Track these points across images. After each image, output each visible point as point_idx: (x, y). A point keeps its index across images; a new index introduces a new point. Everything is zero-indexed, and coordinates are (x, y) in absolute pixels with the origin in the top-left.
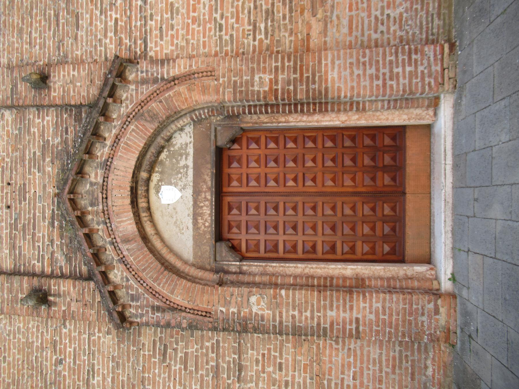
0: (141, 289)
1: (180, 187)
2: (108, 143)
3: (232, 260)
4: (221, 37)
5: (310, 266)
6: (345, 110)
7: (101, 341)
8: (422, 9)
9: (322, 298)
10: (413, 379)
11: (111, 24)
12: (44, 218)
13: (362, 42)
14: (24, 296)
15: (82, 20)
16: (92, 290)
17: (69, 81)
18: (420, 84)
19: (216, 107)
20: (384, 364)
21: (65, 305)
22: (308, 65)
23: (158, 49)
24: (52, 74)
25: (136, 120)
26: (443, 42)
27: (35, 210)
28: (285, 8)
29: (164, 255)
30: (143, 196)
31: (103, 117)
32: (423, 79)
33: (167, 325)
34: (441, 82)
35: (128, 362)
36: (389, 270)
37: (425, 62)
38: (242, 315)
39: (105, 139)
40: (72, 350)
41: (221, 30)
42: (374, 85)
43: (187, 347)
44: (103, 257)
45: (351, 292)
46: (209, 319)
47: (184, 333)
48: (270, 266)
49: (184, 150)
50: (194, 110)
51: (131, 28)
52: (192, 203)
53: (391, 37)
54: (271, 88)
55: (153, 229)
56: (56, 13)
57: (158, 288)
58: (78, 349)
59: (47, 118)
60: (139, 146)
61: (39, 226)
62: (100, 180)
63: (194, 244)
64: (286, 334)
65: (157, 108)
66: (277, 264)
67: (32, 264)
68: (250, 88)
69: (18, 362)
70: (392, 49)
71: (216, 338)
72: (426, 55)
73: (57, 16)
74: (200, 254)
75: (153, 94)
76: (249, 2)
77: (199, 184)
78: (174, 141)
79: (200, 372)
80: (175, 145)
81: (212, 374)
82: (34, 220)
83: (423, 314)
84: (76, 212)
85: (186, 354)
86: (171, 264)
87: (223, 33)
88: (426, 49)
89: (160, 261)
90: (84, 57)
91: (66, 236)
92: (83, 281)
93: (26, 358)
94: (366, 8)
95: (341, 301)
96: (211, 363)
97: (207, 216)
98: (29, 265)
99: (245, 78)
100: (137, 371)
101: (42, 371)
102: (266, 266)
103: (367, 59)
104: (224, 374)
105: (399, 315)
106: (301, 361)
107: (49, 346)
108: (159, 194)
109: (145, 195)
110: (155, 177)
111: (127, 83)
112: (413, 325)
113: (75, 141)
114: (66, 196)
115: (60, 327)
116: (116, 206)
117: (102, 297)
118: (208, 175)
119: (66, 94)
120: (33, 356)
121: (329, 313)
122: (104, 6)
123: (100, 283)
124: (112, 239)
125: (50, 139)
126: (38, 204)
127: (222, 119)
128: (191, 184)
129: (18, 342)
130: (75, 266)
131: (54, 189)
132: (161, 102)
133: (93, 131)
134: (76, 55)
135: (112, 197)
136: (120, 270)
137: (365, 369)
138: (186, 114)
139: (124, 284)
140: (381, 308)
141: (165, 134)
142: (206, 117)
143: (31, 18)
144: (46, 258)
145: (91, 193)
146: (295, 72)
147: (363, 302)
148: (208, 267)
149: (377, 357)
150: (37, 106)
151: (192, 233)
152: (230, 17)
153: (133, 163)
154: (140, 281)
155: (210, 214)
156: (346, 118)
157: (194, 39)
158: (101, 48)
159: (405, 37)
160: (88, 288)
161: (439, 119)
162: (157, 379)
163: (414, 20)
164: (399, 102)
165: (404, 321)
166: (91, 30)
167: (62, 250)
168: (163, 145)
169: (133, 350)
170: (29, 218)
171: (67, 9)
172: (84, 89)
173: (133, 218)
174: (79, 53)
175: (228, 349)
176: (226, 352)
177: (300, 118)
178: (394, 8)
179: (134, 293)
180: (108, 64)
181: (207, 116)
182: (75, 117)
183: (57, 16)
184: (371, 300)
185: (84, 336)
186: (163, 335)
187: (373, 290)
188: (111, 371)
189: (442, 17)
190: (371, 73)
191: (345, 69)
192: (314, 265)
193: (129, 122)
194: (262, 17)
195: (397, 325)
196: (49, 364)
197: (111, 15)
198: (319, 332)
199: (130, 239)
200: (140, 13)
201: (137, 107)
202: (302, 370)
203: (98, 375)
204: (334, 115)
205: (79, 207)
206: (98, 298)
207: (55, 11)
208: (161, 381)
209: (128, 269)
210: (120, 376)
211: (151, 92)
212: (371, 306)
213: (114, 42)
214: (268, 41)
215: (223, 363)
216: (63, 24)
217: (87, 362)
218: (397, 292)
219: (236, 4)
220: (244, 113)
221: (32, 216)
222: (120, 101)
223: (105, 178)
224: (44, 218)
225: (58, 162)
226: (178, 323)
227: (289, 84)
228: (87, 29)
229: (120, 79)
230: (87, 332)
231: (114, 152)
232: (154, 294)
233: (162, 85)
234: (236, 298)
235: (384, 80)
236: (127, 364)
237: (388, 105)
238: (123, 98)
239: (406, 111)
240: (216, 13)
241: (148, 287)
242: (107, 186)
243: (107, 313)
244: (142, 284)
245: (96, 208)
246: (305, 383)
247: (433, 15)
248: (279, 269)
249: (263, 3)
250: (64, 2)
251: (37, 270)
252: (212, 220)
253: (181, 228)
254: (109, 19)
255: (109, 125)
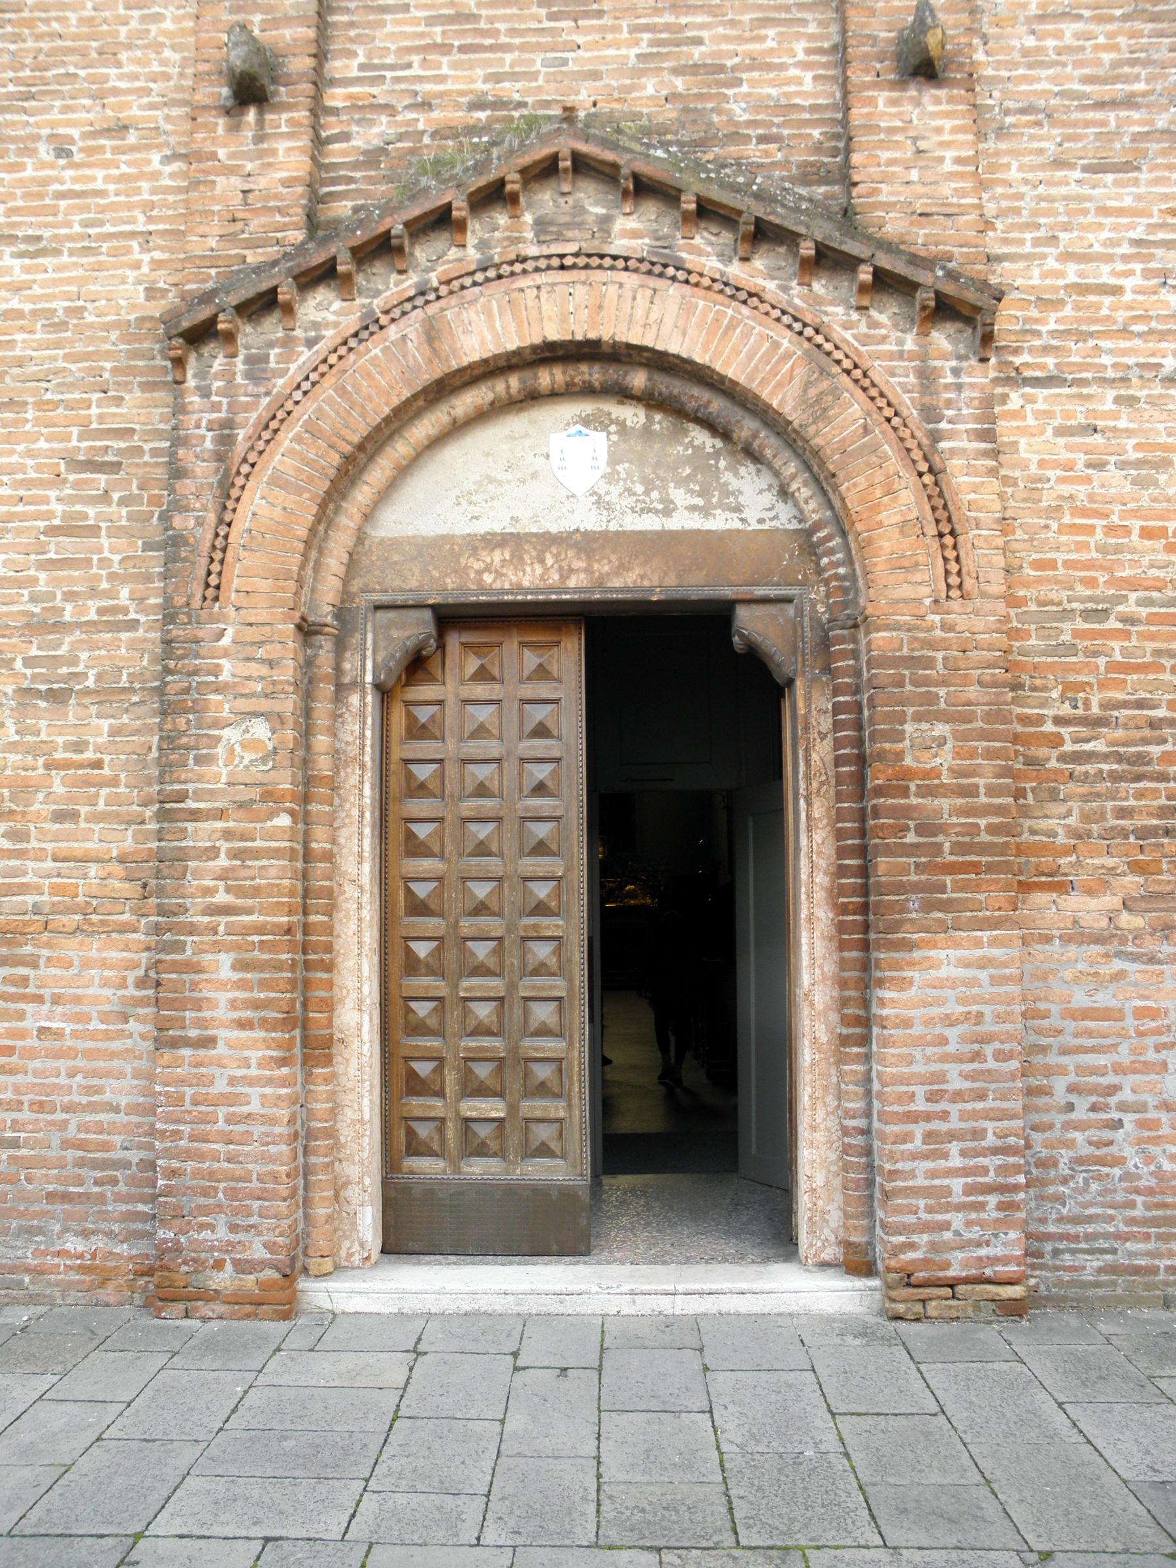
0: (284, 386)
1: (602, 492)
2: (735, 270)
3: (379, 659)
4: (1066, 615)
5: (366, 899)
6: (844, 1003)
7: (128, 272)
8: (1133, 1221)
9: (271, 937)
10: (51, 1197)
11: (1104, 275)
12: (497, 78)
13: (1044, 1050)
14: (256, 32)
15: (1116, 183)
16: (279, 235)
17: (922, 145)
18: (910, 1219)
19: (855, 602)
20: (89, 1118)
21: (232, 156)
22: (977, 888)
23: (1031, 421)
24: (942, 93)
25: (807, 353)
26: (1032, 1282)
27: (523, 48)
28: (1151, 814)
29: (389, 450)
30: (572, 378)
31: (813, 252)
32: (927, 1227)
33: (177, 470)
34: (913, 1280)
35: (66, 357)
36: (359, 1136)
37: (975, 1233)
38: (211, 697)
39: (745, 259)
40: (99, 185)
41: (1087, 615)
42: (912, 1088)
43: (116, 532)
44: (379, 267)
45: (287, 1023)
46: (199, 596)
47: (155, 520)
48: (362, 776)
49: (720, 500)
50: (843, 534)
51: (1091, 334)
52: (554, 529)
53: (1057, 1133)
54: (908, 774)
55: (471, 411)
56: (1139, 99)
57: (286, 439)
58: (102, 202)
59: (808, 76)
60: (727, 363)
61: (471, 66)
62: (618, 245)
63: (424, 538)
64: (160, 831)
65: (845, 419)
66: (368, 801)
67: (354, 47)
68: (910, 710)
69: (58, 19)
70: (1016, 1135)
71: (143, 619)
72: (996, 1236)
73: (1129, 102)
74: (396, 558)
75: (889, 404)
76: (1173, 705)
77: (614, 552)
78: (747, 469)
79: (43, 576)
80: (736, 474)
81: (37, 610)
82: (492, 48)
83: (234, 1228)
84: (517, 177)
85: (94, 531)
86: (362, 471)
87: (1081, 625)
88: (1013, 1235)
89: (368, 438)
90: (999, 190)
91: (442, 148)
92: (304, 207)
93: (69, 43)
94: (1142, 1059)
95: (262, 995)
96: (69, 607)
97: (514, 579)
98: (352, 40)
99: (942, 692)
100: (44, 385)
101: (30, 97)
102: (362, 766)
103: (991, 1064)
104: (39, 648)
105: (229, 1161)
106: (85, 876)
107: (109, 113)
108: (579, 427)
109: (575, 385)
110: (633, 415)
111: (920, 326)
112: (202, 1201)
113: (739, 165)
114: (565, 145)
115: (167, 144)
116: (538, 297)
117: (258, 270)
118: (642, 577)
119: (882, 136)
120: (76, 66)
121: (225, 959)
122: (1159, 252)
123: (301, 260)
124: (436, 290)
125: (745, 88)
126: (538, 58)
127: (819, 620)
128: (613, 527)
129: (118, 17)
130: (351, 180)
131: (588, 104)
132: (866, 430)
133: (770, 223)
134: (1008, 166)
135: (567, 284)
136: (341, 319)
137: (71, 1063)
138: (831, 507)
139: (298, 333)
140: (245, 1109)
141: (768, 443)
142: (824, 570)
143: (1125, 18)
144: (374, 90)
145: (578, 219)
146: (958, 848)
147: (263, 1058)
148: (355, 586)
149: (107, 1096)
150: (845, 48)
151: (458, 532)
152: (1126, 644)
153: (674, 345)
154: (307, 385)
155: (519, 588)
156: (819, 1007)
157: (1060, 532)
158: (1028, 244)
159: (1053, 1173)
160: (285, 224)
161: (808, 1275)
162: (21, 448)
163: (1100, 1199)
164: (863, 1160)
165: (211, 1175)
166: (1085, 212)
167: (401, 137)
168: (735, 436)
169: (102, 369)
170: (498, 31)
171: (1148, 133)
172: (899, 193)
173: (501, 350)
174: (1014, 174)
175: (110, 658)
176: (103, 652)
177: (823, 863)
178: (1140, 1141)
179: (272, 365)
180: (978, 267)
181: (826, 575)
182: (812, 164)
183: (1129, 102)
184: (270, 1081)
185: (141, 218)
186: (147, 458)
187: (298, 1087)
188: (39, 306)
189: (1104, 1278)
190: (948, 1077)
191: (961, 1001)
192: (370, 913)
193: (800, 333)
194: (1125, 744)
195: (200, 1157)
196: (55, 115)
197: (1129, 273)
198: (169, 930)
199: (436, 345)
200: (1137, 365)
201: (847, 356)
202: (58, 880)
203: (27, 270)
204: (829, 968)
205: (534, 186)
206: (253, 257)
207: (1144, 94)
208: (14, 459)
209: (345, 343)
210: (26, 336)
211: (893, 401)
212: (251, 1082)
213: (1048, 282)
214: (1053, 764)
215: (72, 643)
216: (1103, 123)
217: (63, 231)
218: (295, 1158)
219: (1168, 663)
220: (836, 691)
221: (504, 39)
222: (865, 302)
223: (624, 262)
224: (497, 78)
225: (674, 115)
226: (184, 503)
227: (921, 830)
228: (1089, 199)
229: (932, 304)
230: (152, 228)
231: (709, 288)
232: (271, 427)
233: (918, 434)
234: (262, 678)
235: (928, 1117)
236: (61, 352)
237: (854, 1128)
238: (873, 313)
239: (837, 1182)
240: (1139, 603)
241: (289, 405)
242: (600, 267)
243: (210, 285)
244: (298, 387)
245: (530, 235)
246: (24, 889)
247: (1114, 1251)
248: (353, 805)
249: (1168, 747)
250: (1171, 122)
251: (337, 64)
252: (503, 592)
253: (474, 498)
254: (1120, 266)
255: (791, 270)
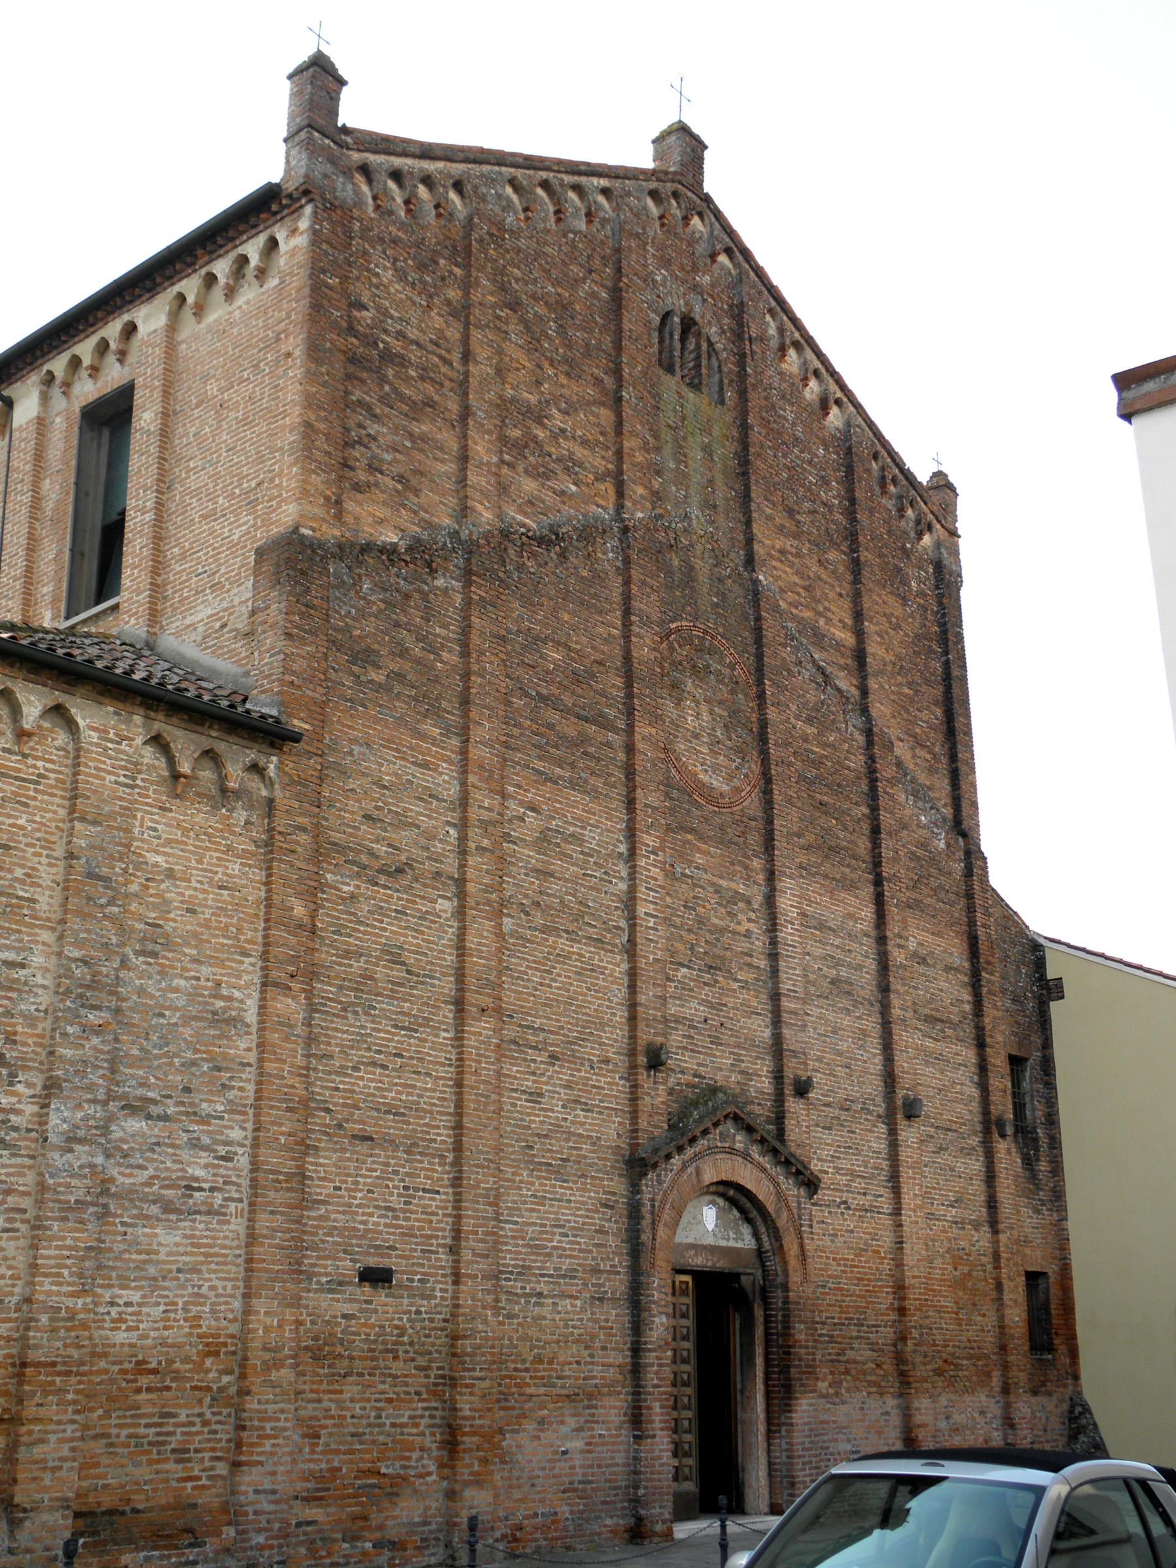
43: (614, 1234)
121: (657, 1404)
246: (594, 1377)
